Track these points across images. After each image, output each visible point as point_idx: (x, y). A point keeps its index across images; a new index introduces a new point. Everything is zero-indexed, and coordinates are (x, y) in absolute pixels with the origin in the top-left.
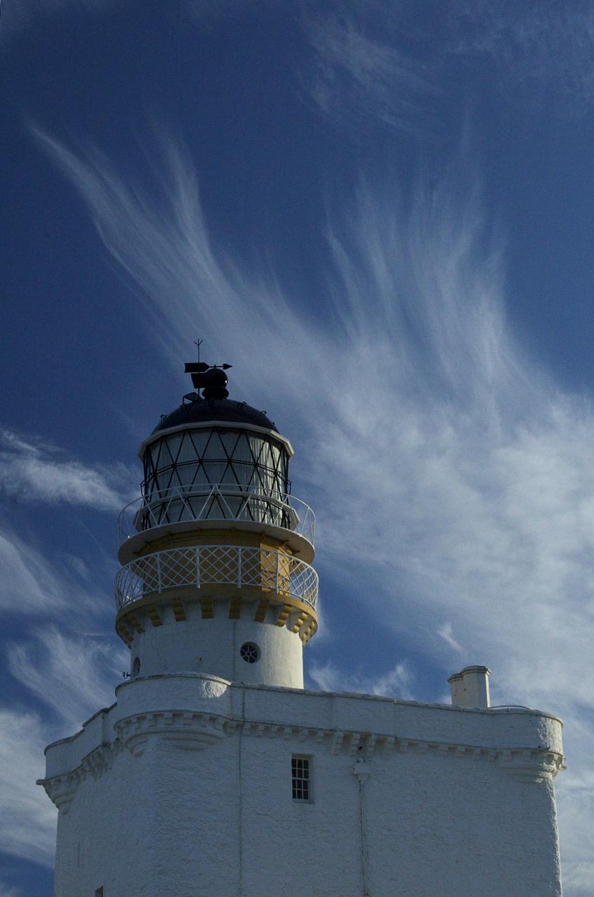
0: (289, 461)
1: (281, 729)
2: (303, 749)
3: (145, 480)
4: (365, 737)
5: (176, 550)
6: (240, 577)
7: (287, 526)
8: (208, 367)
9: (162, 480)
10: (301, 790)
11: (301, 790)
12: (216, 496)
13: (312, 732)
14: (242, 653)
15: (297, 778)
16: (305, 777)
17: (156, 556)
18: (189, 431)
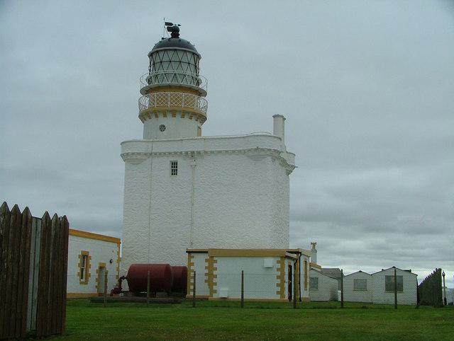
1: (160, 154)
2: (174, 159)
4: (193, 152)
9: (157, 66)
10: (174, 171)
11: (174, 171)
12: (175, 74)
13: (176, 153)
18: (176, 50)
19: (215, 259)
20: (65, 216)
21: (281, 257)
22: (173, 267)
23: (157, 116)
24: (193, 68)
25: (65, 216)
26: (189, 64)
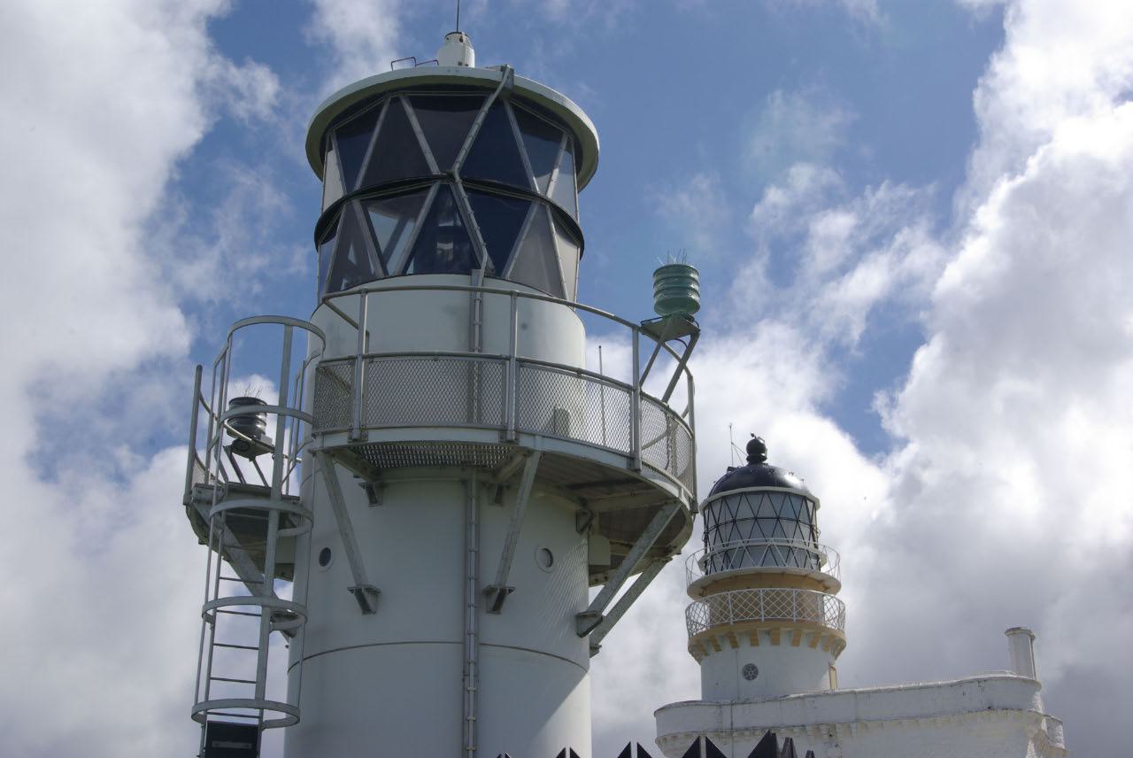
6: (763, 613)
23: (735, 645)
26: (778, 518)
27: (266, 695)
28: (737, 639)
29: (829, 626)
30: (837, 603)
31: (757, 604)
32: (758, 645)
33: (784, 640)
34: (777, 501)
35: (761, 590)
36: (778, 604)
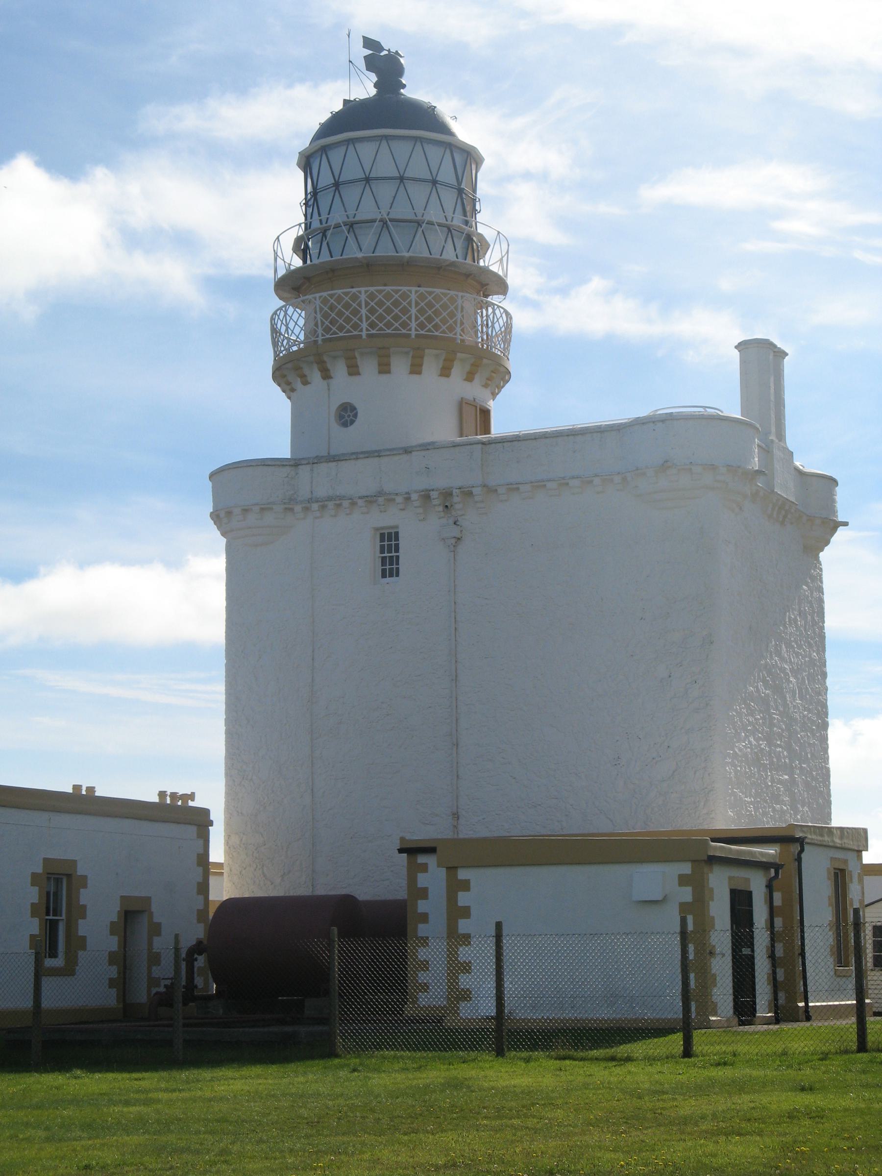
0: (479, 174)
3: (306, 199)
4: (447, 494)
5: (339, 292)
7: (476, 262)
8: (383, 49)
14: (352, 422)
15: (386, 555)
16: (395, 552)
17: (360, 292)
18: (349, 142)
19: (462, 874)
20: (736, 347)
21: (693, 861)
22: (363, 901)
24: (449, 197)
25: (736, 347)
26: (434, 182)
27: (868, 877)
28: (329, 366)
29: (302, 337)
30: (504, 315)
31: (405, 311)
32: (358, 373)
33: (430, 367)
34: (434, 153)
35: (363, 289)
36: (388, 311)
